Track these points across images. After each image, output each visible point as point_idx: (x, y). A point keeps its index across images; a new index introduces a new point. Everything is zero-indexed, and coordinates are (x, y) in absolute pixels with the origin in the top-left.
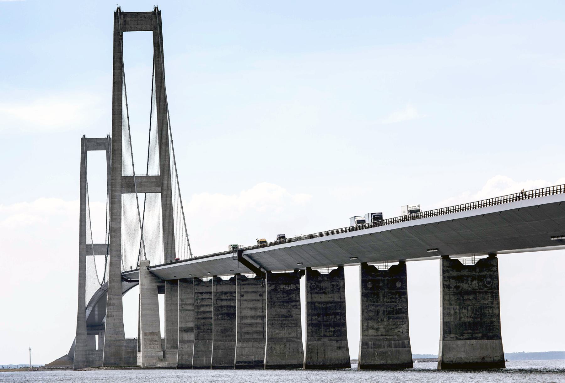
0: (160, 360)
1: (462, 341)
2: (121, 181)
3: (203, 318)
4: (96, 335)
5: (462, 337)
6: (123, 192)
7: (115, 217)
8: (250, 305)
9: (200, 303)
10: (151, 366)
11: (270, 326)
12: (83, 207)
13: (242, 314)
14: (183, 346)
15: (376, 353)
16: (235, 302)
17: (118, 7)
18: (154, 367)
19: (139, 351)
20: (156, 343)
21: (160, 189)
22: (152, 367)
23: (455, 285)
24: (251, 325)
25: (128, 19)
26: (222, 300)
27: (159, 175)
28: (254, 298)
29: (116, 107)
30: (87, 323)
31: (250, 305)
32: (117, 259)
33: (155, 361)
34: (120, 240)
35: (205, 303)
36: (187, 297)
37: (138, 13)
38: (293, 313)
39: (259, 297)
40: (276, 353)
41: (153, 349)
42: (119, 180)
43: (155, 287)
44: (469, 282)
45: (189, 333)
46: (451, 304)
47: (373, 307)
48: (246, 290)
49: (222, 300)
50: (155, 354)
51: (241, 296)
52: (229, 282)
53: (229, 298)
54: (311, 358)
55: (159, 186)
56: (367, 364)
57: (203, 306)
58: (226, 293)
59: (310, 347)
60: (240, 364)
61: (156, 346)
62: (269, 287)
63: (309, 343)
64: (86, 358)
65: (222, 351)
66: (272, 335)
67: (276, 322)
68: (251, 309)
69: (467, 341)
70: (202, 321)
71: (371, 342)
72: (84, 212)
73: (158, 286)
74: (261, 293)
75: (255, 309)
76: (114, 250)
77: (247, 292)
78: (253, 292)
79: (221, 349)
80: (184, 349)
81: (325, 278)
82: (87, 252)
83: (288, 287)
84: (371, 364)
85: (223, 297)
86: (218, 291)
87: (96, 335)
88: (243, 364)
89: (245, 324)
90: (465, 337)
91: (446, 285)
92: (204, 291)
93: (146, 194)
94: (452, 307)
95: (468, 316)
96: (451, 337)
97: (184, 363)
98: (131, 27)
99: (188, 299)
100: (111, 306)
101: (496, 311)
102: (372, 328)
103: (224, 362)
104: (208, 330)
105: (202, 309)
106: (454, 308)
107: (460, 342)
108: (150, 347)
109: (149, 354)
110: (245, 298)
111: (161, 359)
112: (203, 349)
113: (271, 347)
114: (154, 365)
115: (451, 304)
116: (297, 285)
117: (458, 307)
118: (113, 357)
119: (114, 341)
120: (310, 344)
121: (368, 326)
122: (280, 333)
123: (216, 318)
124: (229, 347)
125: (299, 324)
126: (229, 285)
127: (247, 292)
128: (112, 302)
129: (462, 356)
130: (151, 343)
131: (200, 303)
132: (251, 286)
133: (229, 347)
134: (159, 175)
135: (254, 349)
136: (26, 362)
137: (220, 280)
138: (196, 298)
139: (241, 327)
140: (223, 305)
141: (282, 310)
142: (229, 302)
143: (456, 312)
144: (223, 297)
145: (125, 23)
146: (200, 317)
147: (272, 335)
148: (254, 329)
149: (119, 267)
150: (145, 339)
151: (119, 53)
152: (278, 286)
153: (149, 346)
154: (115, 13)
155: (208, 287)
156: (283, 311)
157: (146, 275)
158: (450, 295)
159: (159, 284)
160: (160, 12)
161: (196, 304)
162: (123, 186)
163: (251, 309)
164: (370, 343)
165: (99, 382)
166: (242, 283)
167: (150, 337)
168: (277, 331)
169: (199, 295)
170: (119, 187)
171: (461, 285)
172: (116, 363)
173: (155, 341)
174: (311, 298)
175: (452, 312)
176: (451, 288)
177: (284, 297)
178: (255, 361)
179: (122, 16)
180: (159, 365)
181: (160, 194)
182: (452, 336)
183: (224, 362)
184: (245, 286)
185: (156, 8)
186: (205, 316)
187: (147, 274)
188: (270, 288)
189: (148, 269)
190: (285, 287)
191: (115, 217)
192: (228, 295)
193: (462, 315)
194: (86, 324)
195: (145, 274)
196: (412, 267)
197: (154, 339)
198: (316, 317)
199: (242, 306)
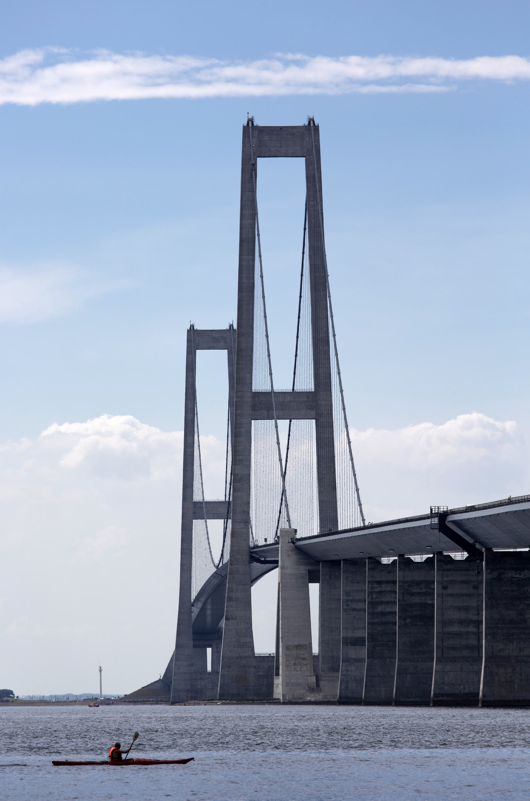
0: (311, 690)
2: (251, 399)
3: (381, 624)
7: (240, 457)
9: (377, 598)
10: (296, 699)
17: (250, 117)
18: (302, 700)
19: (278, 674)
20: (305, 662)
21: (313, 413)
24: (459, 635)
25: (266, 138)
27: (313, 391)
29: (245, 280)
32: (242, 525)
33: (302, 692)
35: (384, 599)
40: (499, 680)
49: (412, 594)
52: (425, 565)
53: (424, 590)
57: (382, 603)
58: (418, 583)
60: (440, 698)
68: (459, 609)
70: (380, 628)
73: (309, 570)
75: (467, 609)
77: (453, 582)
78: (462, 582)
80: (350, 673)
82: (194, 513)
83: (520, 574)
85: (415, 590)
88: (445, 698)
89: (449, 633)
92: (384, 579)
93: (290, 421)
98: (270, 150)
105: (380, 609)
108: (295, 669)
109: (293, 681)
110: (449, 591)
113: (492, 672)
114: (301, 699)
123: (403, 623)
127: (453, 582)
130: (297, 662)
131: (377, 598)
134: (313, 391)
136: (93, 690)
140: (414, 601)
142: (424, 598)
144: (415, 590)
149: (245, 540)
150: (286, 655)
152: (503, 572)
154: (244, 127)
155: (389, 572)
157: (290, 553)
159: (309, 568)
160: (318, 126)
163: (459, 609)
166: (445, 567)
168: (501, 646)
173: (304, 659)
177: (512, 591)
181: (314, 421)
185: (311, 121)
187: (292, 551)
188: (490, 576)
189: (294, 543)
190: (515, 574)
191: (240, 457)
194: (191, 630)
195: (288, 551)
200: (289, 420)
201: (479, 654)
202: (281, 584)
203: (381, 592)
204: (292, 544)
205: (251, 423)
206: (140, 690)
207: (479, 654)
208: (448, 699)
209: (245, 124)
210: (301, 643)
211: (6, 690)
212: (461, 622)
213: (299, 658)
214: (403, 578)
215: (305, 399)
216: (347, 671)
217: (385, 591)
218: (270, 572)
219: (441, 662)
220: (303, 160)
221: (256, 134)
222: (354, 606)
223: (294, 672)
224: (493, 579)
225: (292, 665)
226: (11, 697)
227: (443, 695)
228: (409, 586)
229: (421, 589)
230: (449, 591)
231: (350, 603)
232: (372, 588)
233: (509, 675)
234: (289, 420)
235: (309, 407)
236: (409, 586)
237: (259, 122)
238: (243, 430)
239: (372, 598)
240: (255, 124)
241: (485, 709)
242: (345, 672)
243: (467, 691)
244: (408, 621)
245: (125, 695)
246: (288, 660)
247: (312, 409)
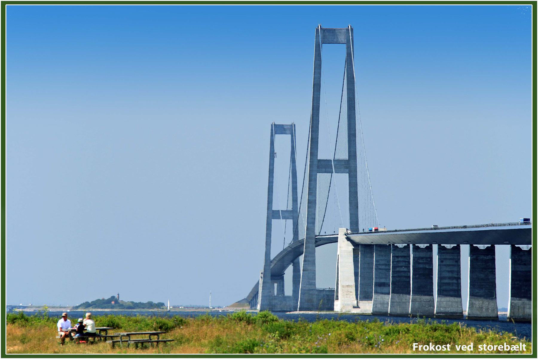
2: (317, 163)
3: (399, 277)
4: (275, 284)
6: (318, 172)
7: (311, 191)
8: (448, 269)
9: (396, 264)
10: (347, 311)
12: (271, 180)
13: (441, 276)
14: (377, 298)
16: (395, 263)
19: (337, 299)
20: (351, 294)
21: (347, 170)
24: (449, 284)
25: (327, 34)
26: (419, 263)
27: (347, 159)
28: (451, 263)
29: (315, 104)
30: (271, 274)
31: (448, 269)
32: (312, 225)
33: (350, 308)
34: (315, 210)
35: (399, 265)
36: (381, 258)
38: (489, 277)
39: (454, 263)
40: (476, 307)
41: (349, 299)
42: (316, 163)
45: (382, 287)
48: (445, 257)
49: (419, 263)
50: (350, 303)
51: (441, 261)
52: (425, 249)
53: (425, 262)
54: (513, 313)
57: (398, 267)
58: (422, 258)
59: (513, 304)
60: (439, 314)
61: (351, 296)
63: (512, 301)
64: (270, 303)
65: (418, 303)
67: (476, 284)
68: (449, 272)
70: (398, 279)
72: (271, 184)
74: (457, 260)
75: (452, 272)
76: (310, 218)
77: (446, 259)
78: (450, 259)
79: (418, 302)
80: (378, 300)
81: (526, 254)
82: (273, 216)
83: (486, 257)
85: (421, 261)
86: (417, 256)
87: (275, 284)
88: (441, 314)
89: (443, 283)
92: (400, 255)
97: (378, 310)
98: (329, 40)
99: (381, 260)
101: (459, 264)
103: (419, 312)
104: (402, 286)
105: (398, 269)
109: (345, 303)
110: (444, 263)
112: (398, 301)
113: (472, 303)
116: (493, 256)
118: (306, 303)
122: (479, 292)
123: (414, 277)
124: (424, 300)
125: (494, 286)
126: (425, 252)
127: (446, 259)
128: (307, 259)
130: (348, 293)
131: (396, 264)
132: (449, 254)
133: (424, 300)
134: (347, 159)
135: (450, 303)
137: (418, 247)
139: (440, 286)
140: (420, 267)
141: (482, 275)
142: (425, 265)
144: (421, 261)
145: (324, 37)
146: (395, 275)
148: (451, 288)
150: (343, 290)
151: (319, 61)
152: (478, 256)
153: (346, 296)
155: (402, 252)
156: (482, 276)
162: (318, 167)
163: (449, 272)
166: (442, 252)
167: (347, 289)
168: (477, 291)
169: (396, 258)
170: (315, 168)
173: (351, 292)
174: (515, 268)
177: (483, 265)
178: (451, 313)
181: (348, 174)
183: (419, 312)
184: (444, 254)
186: (399, 275)
190: (484, 257)
191: (311, 191)
192: (424, 259)
194: (270, 275)
196: (462, 246)
198: (518, 282)
199: (442, 270)
202: (340, 255)
203: (398, 261)
205: (317, 175)
208: (443, 315)
210: (350, 284)
212: (450, 278)
213: (349, 291)
214: (415, 255)
215: (344, 164)
216: (376, 299)
217: (400, 261)
218: (320, 246)
221: (322, 32)
222: (380, 267)
223: (346, 299)
224: (473, 259)
225: (345, 295)
227: (440, 313)
228: (418, 260)
229: (423, 261)
230: (444, 263)
231: (378, 266)
232: (394, 259)
233: (481, 304)
235: (345, 167)
236: (418, 260)
238: (313, 178)
239: (394, 264)
242: (375, 299)
243: (452, 311)
244: (417, 276)
247: (347, 168)
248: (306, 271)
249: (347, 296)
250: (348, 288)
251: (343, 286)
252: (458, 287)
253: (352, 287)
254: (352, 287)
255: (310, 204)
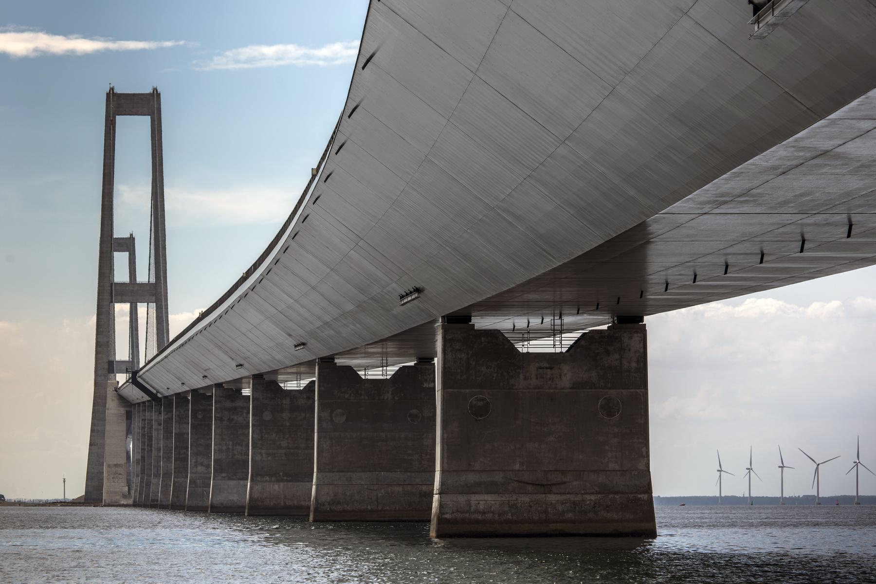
0: (124, 496)
1: (235, 481)
5: (234, 477)
7: (101, 329)
10: (113, 502)
11: (165, 459)
15: (205, 493)
17: (111, 87)
18: (117, 504)
20: (121, 476)
22: (114, 504)
23: (228, 417)
29: (106, 203)
32: (103, 378)
33: (118, 497)
37: (134, 95)
43: (123, 412)
44: (245, 414)
46: (223, 439)
47: (203, 441)
50: (118, 490)
55: (153, 295)
56: (194, 505)
62: (166, 415)
66: (167, 470)
69: (240, 481)
71: (200, 480)
73: (126, 411)
76: (99, 368)
84: (199, 505)
90: (238, 477)
91: (218, 417)
93: (148, 304)
94: (224, 442)
95: (242, 454)
96: (222, 477)
98: (125, 111)
100: (94, 432)
102: (202, 464)
106: (226, 444)
107: (232, 483)
108: (113, 481)
109: (111, 490)
111: (125, 496)
114: (117, 502)
115: (223, 439)
117: (231, 443)
119: (98, 473)
120: (176, 482)
121: (196, 462)
129: (235, 499)
138: (143, 425)
143: (228, 449)
147: (167, 470)
149: (104, 388)
150: (108, 471)
154: (107, 94)
157: (114, 398)
158: (222, 428)
159: (127, 409)
160: (160, 94)
161: (143, 432)
164: (198, 481)
165: (559, 583)
167: (114, 469)
171: (236, 417)
172: (99, 499)
173: (120, 474)
174: (180, 429)
175: (224, 448)
176: (224, 420)
179: (115, 98)
180: (122, 502)
181: (155, 304)
182: (224, 475)
187: (115, 397)
188: (166, 417)
189: (117, 391)
191: (101, 329)
193: (235, 452)
195: (112, 397)
197: (119, 472)
200: (146, 303)
201: (157, 472)
204: (115, 392)
206: (759, 497)
207: (157, 472)
209: (108, 92)
210: (119, 463)
211: (845, 495)
213: (117, 473)
215: (148, 288)
219: (156, 477)
220: (149, 117)
223: (113, 484)
226: (2, 500)
234: (146, 303)
237: (118, 90)
240: (115, 91)
241: (136, 510)
245: (73, 499)
246: (109, 475)
248: (95, 445)
249: (114, 480)
250: (116, 469)
251: (109, 466)
252: (158, 463)
253: (122, 467)
254: (122, 467)
255: (100, 347)
